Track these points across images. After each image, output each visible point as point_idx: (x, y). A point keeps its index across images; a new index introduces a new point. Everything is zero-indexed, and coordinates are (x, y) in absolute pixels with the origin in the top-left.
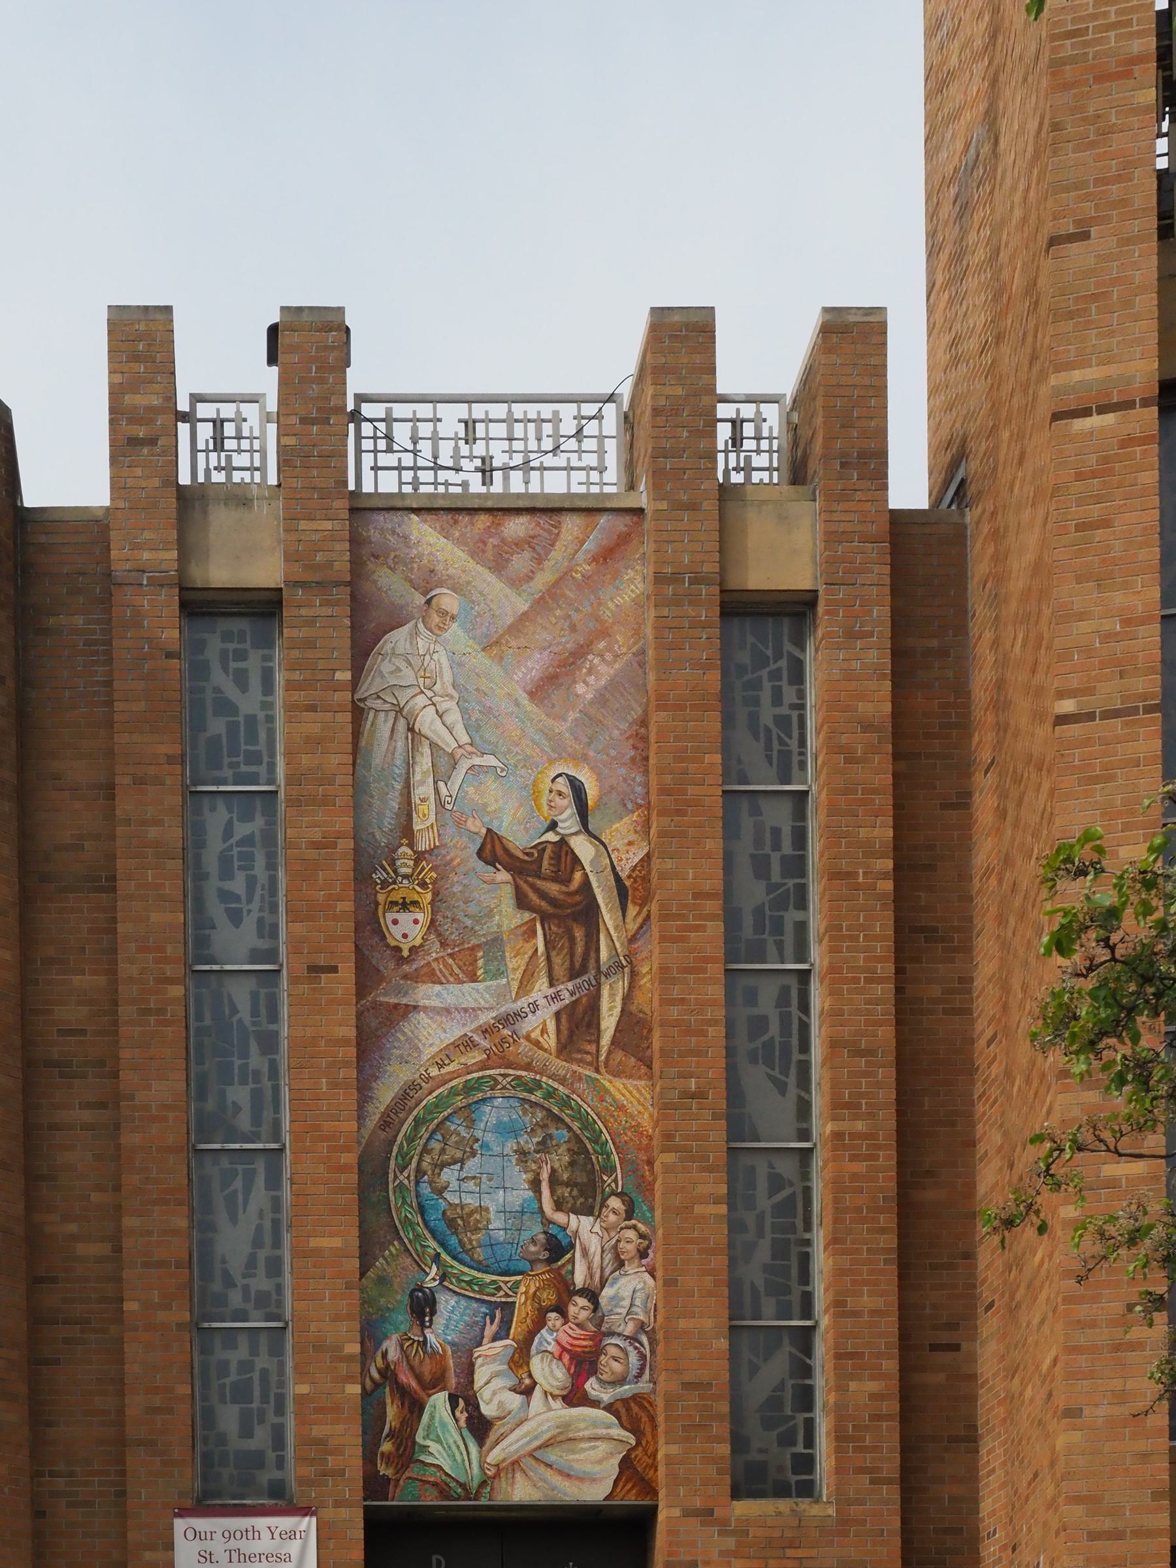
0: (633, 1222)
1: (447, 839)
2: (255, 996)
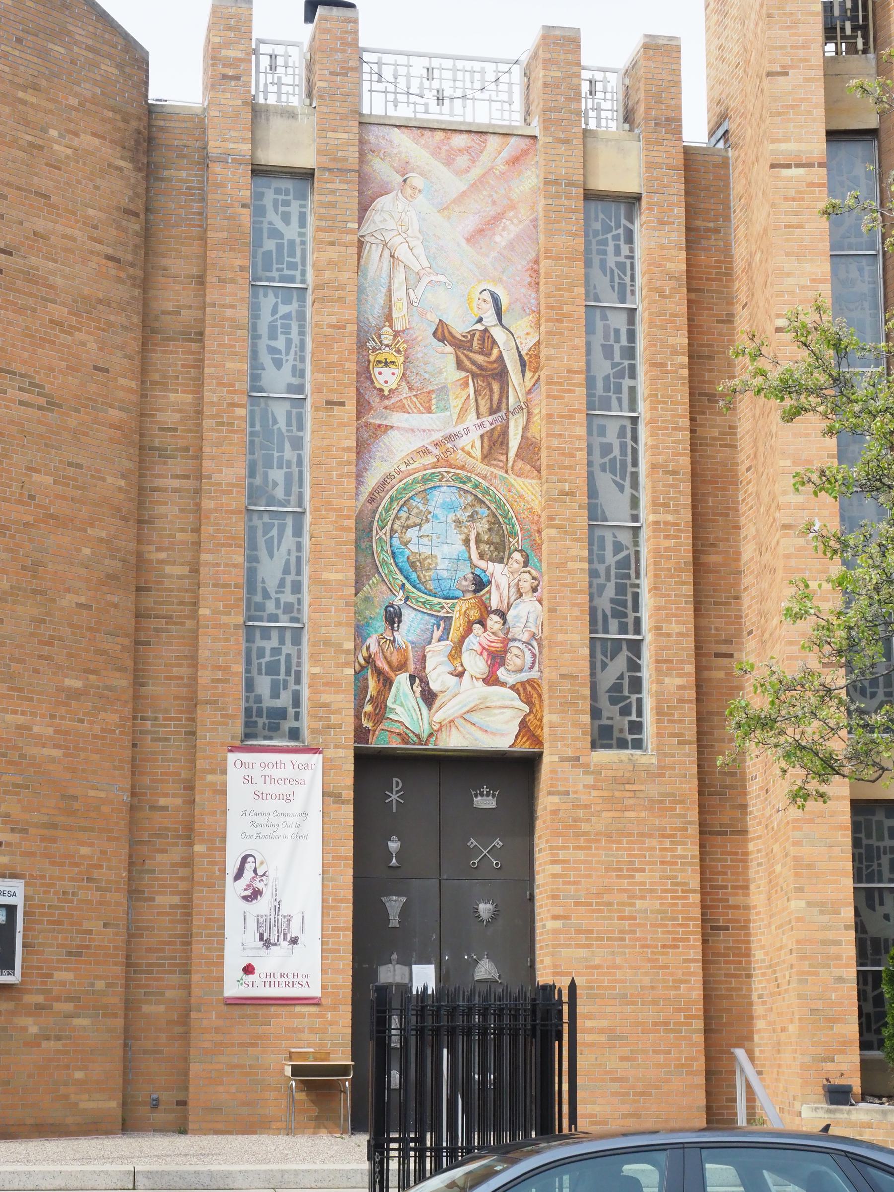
0: (528, 569)
1: (414, 325)
2: (289, 414)
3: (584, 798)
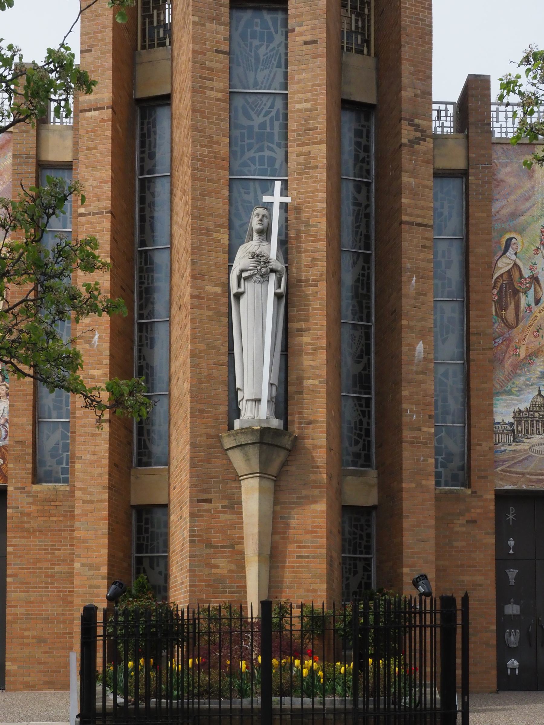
3: (27, 510)
